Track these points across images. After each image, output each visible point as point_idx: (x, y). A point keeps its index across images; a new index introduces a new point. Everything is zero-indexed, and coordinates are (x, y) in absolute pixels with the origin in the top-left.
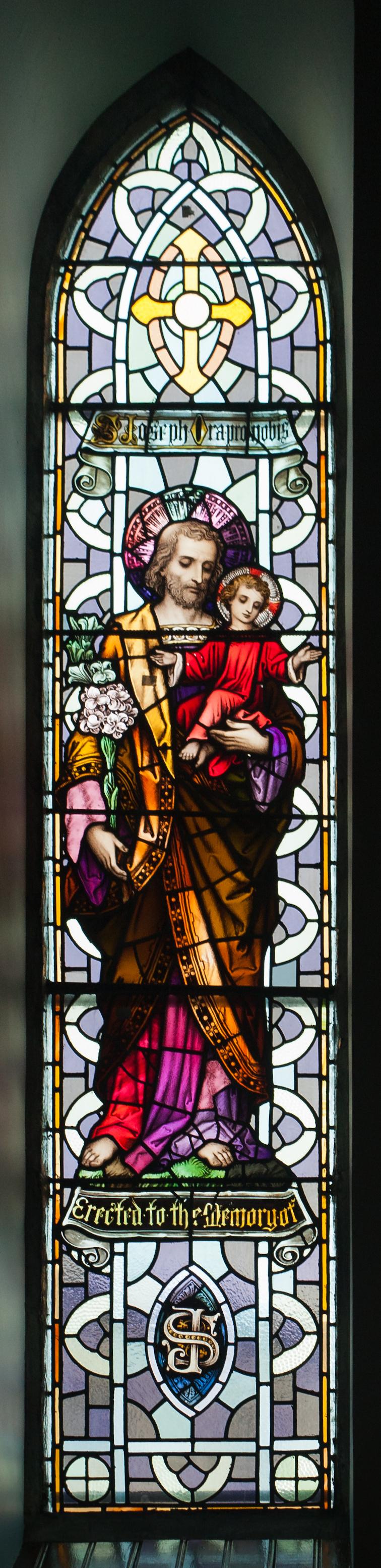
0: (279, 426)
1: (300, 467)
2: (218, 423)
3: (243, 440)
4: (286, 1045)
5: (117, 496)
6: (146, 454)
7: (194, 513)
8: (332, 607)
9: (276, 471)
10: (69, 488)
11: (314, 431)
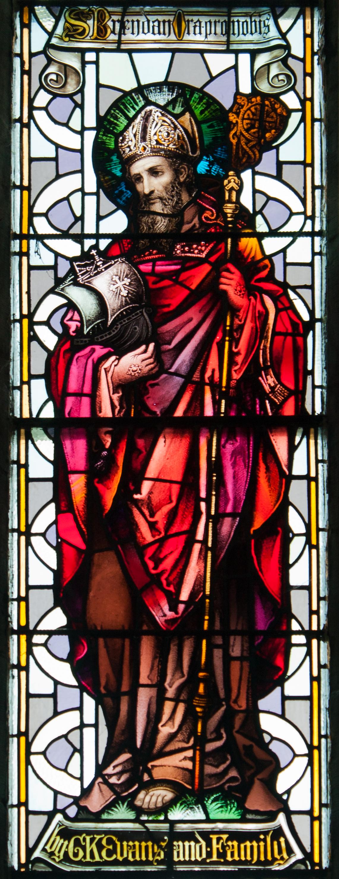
0: (260, 21)
1: (284, 61)
2: (195, 19)
3: (224, 35)
4: (272, 195)
5: (85, 730)
6: (118, 50)
7: (170, 100)
8: (326, 737)
9: (257, 66)
10: (35, 85)
11: (300, 22)
